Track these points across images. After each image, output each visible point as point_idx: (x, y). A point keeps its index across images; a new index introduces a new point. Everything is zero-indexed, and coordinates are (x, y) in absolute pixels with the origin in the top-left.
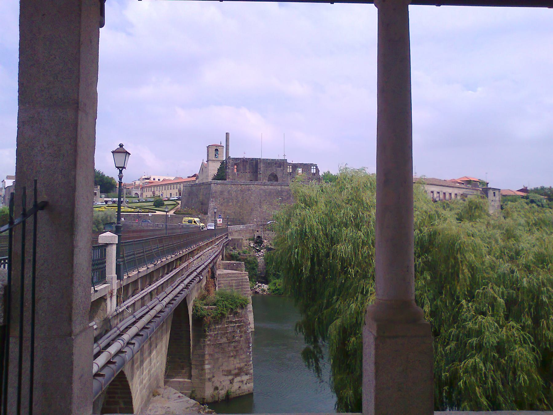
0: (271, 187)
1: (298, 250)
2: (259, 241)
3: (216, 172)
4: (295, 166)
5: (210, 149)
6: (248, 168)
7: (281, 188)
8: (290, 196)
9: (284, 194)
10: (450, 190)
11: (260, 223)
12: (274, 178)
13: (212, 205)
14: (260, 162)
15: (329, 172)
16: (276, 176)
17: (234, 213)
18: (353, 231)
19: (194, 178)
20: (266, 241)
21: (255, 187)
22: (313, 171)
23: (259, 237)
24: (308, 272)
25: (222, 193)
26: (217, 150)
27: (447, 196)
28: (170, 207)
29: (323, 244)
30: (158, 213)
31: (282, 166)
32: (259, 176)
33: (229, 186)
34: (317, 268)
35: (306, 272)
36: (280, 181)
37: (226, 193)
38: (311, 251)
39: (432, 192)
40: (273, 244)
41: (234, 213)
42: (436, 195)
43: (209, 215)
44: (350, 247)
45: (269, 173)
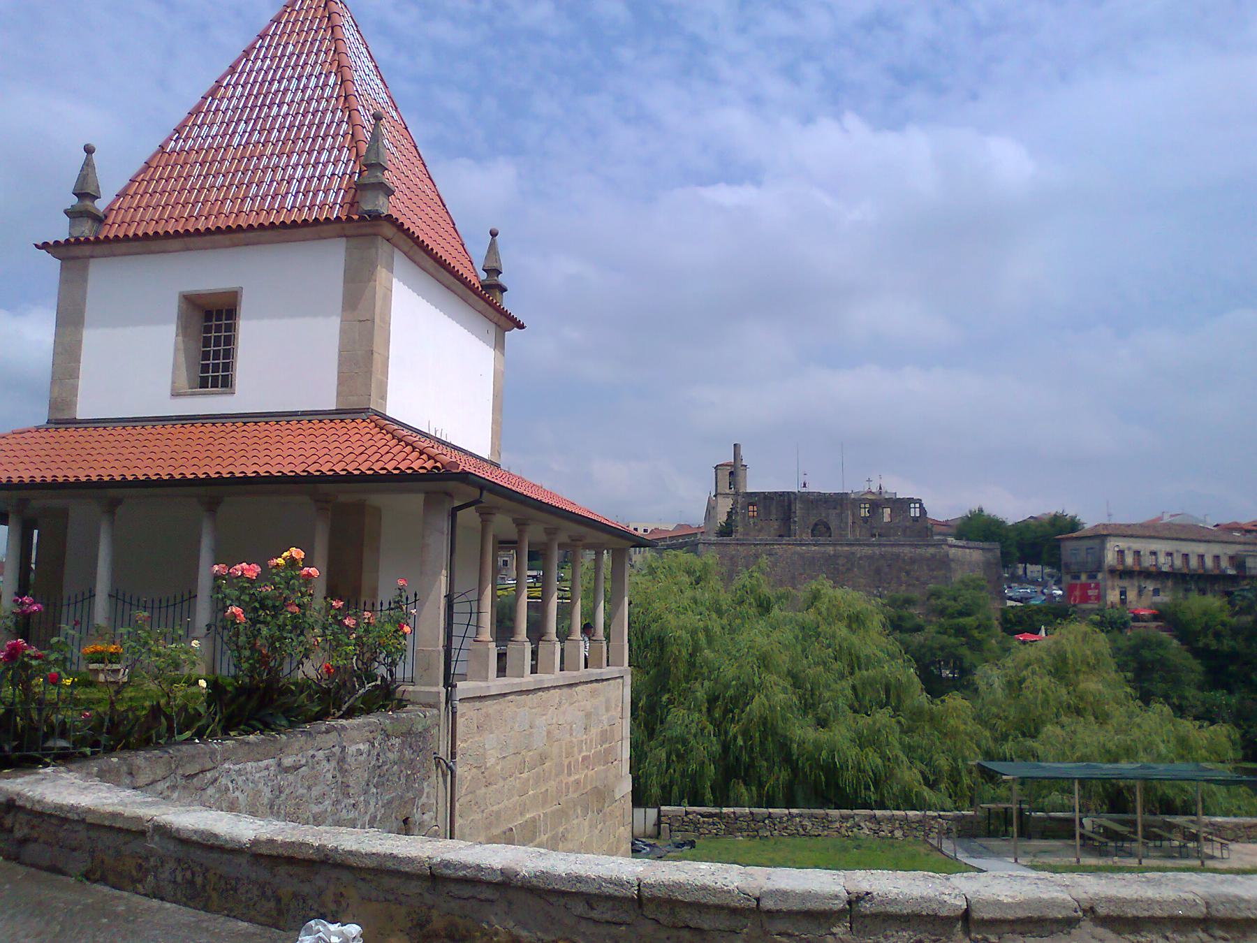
6: (774, 511)
8: (852, 565)
10: (1201, 548)
15: (981, 510)
22: (914, 512)
27: (1194, 563)
33: (732, 547)
39: (1154, 553)
42: (1162, 559)
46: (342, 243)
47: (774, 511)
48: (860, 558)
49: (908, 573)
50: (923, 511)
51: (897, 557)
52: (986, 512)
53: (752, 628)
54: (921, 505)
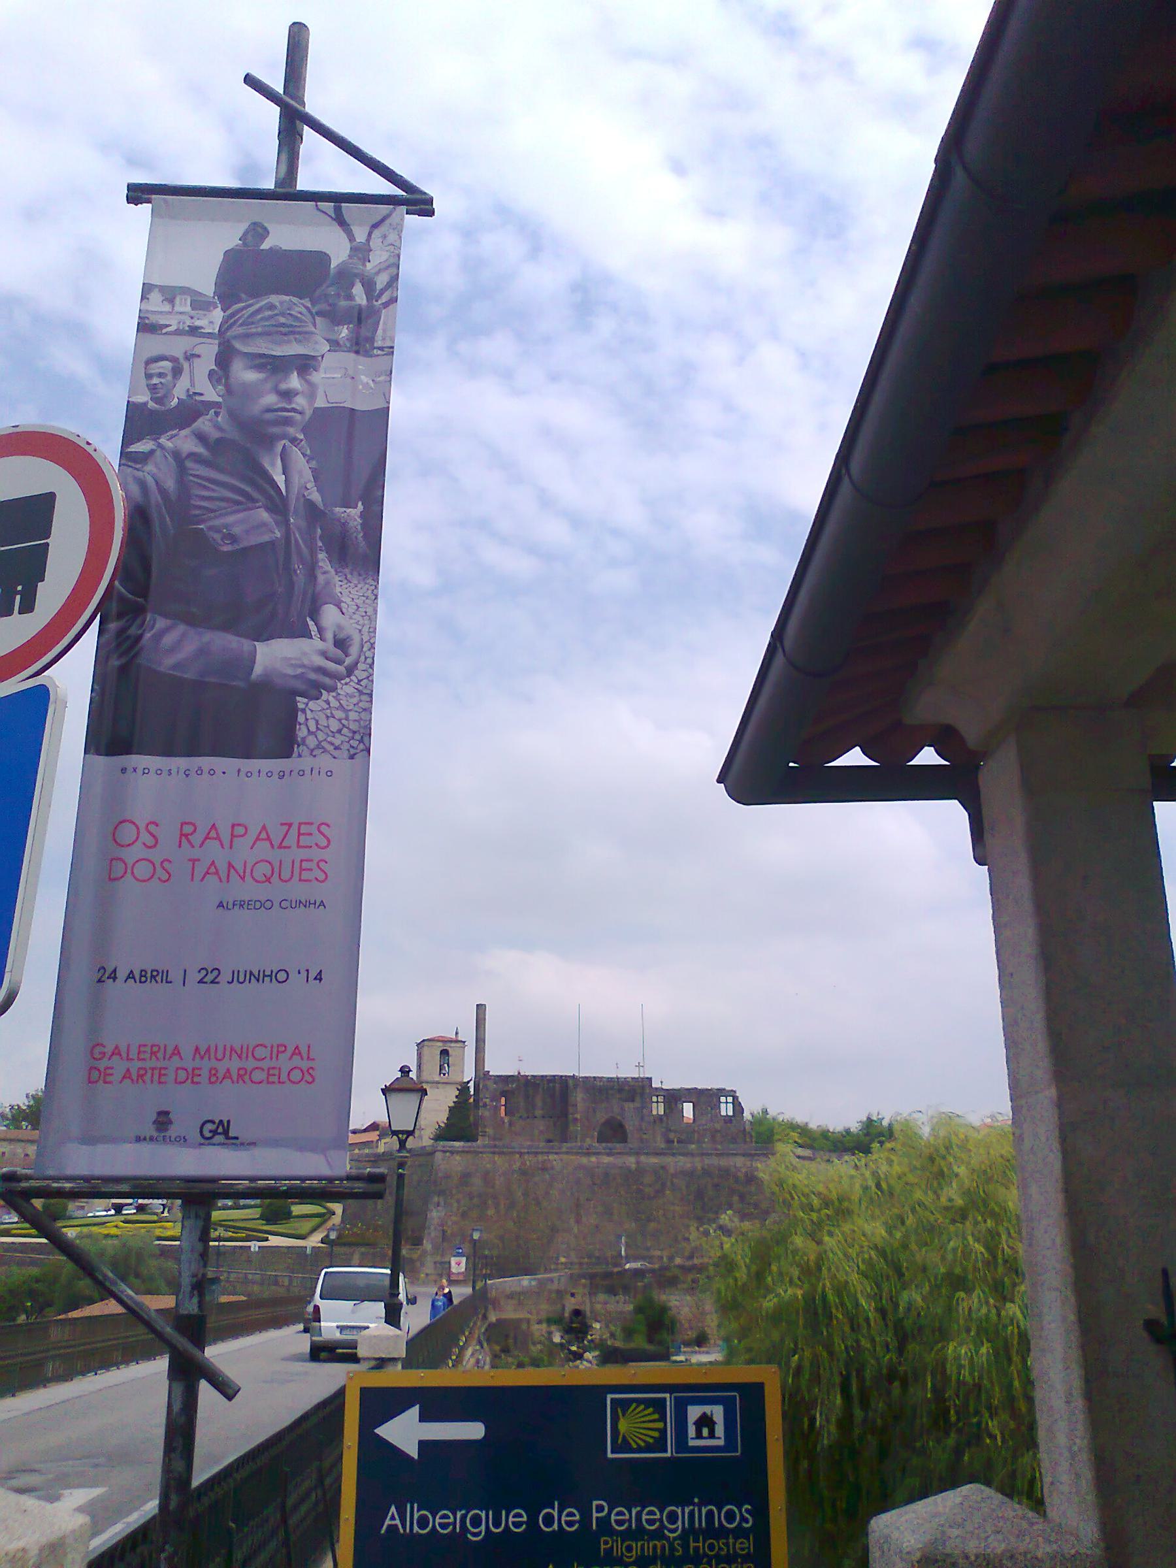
0: (606, 1160)
1: (801, 1359)
2: (576, 1326)
3: (443, 1117)
4: (674, 1098)
5: (426, 1051)
6: (539, 1103)
7: (638, 1163)
8: (664, 1185)
9: (648, 1179)
11: (576, 1270)
12: (614, 1132)
13: (435, 1215)
14: (576, 1086)
15: (765, 1112)
16: (621, 1126)
17: (501, 1238)
18: (987, 1303)
19: (373, 1136)
20: (597, 1326)
21: (561, 1161)
22: (726, 1109)
23: (577, 1313)
24: (833, 1428)
25: (465, 1177)
26: (445, 1053)
28: (307, 1226)
29: (873, 1341)
30: (274, 1241)
31: (638, 1099)
32: (571, 1128)
34: (858, 1413)
35: (829, 1434)
36: (633, 1143)
37: (477, 1182)
38: (841, 1364)
40: (618, 1333)
41: (501, 1238)
43: (427, 1245)
44: (984, 1350)
45: (601, 1117)
46: (404, 1218)
47: (539, 1103)
48: (674, 1175)
49: (742, 1198)
50: (738, 1108)
51: (725, 1173)
52: (772, 1112)
53: (999, 1541)
54: (735, 1098)
